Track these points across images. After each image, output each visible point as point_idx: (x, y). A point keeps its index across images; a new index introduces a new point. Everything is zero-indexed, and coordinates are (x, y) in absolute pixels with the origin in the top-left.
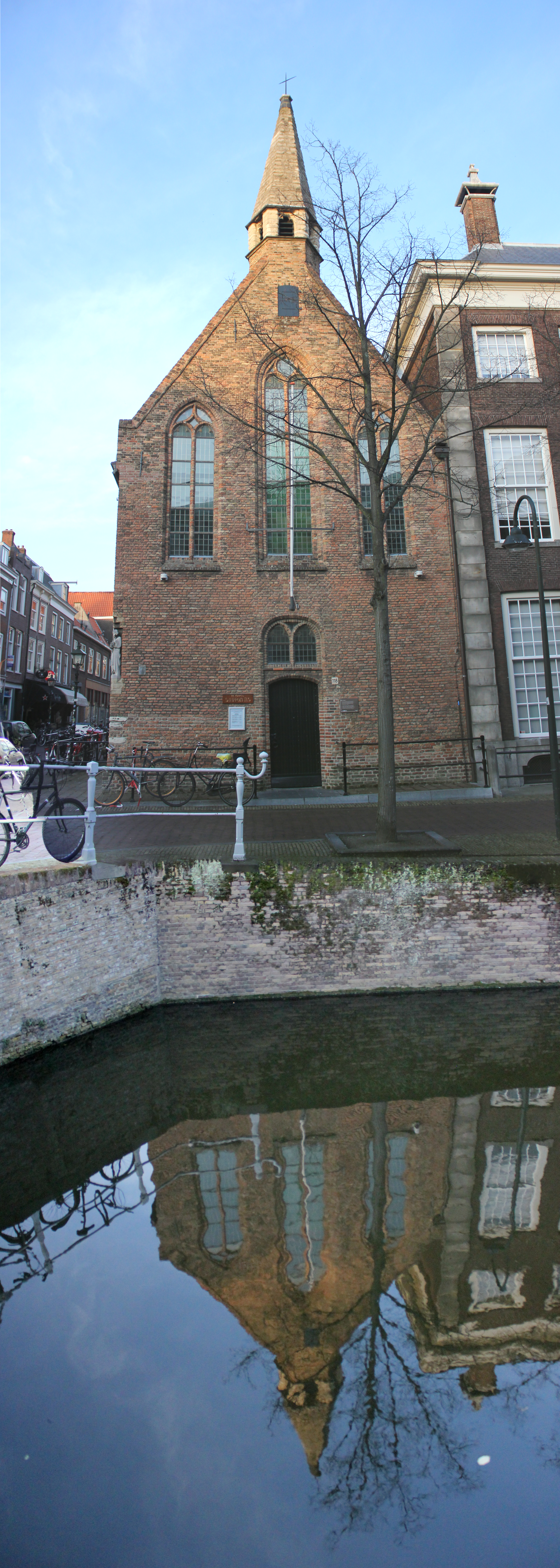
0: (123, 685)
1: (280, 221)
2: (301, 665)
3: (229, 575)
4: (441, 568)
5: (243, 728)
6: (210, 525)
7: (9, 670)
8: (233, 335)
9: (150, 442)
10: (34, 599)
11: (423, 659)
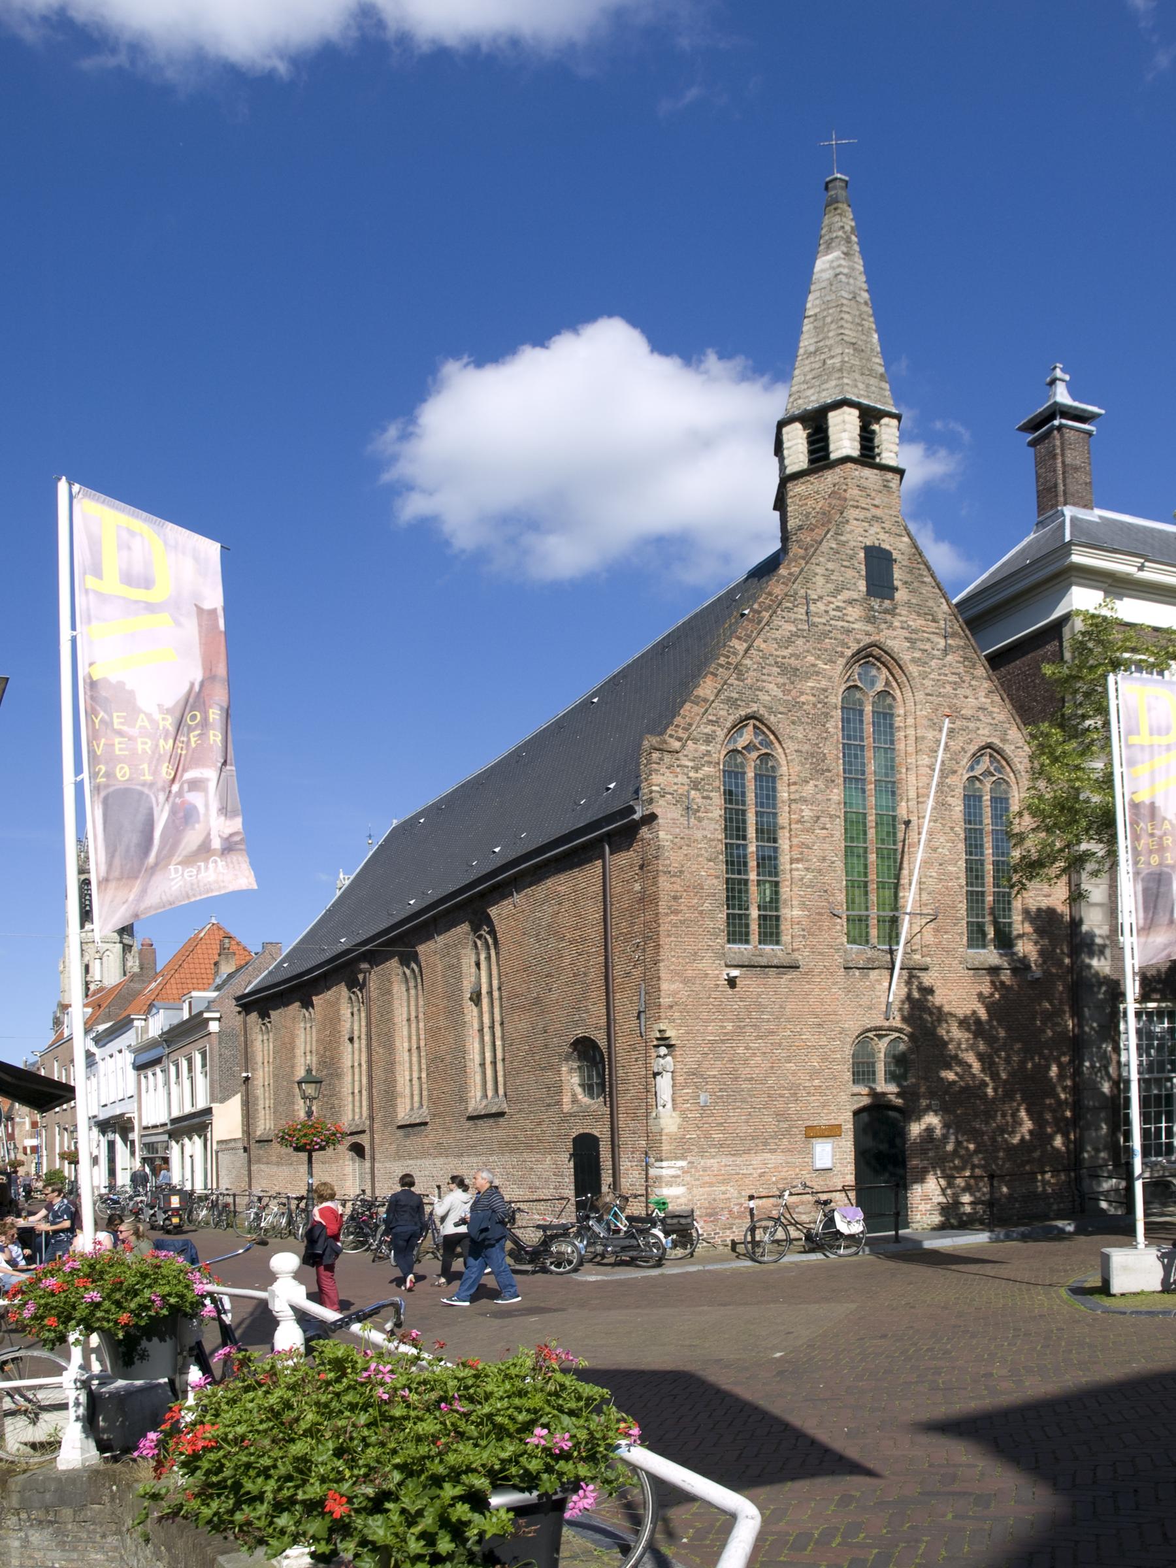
0: (679, 1120)
3: (811, 971)
5: (829, 1165)
8: (804, 617)
9: (699, 775)
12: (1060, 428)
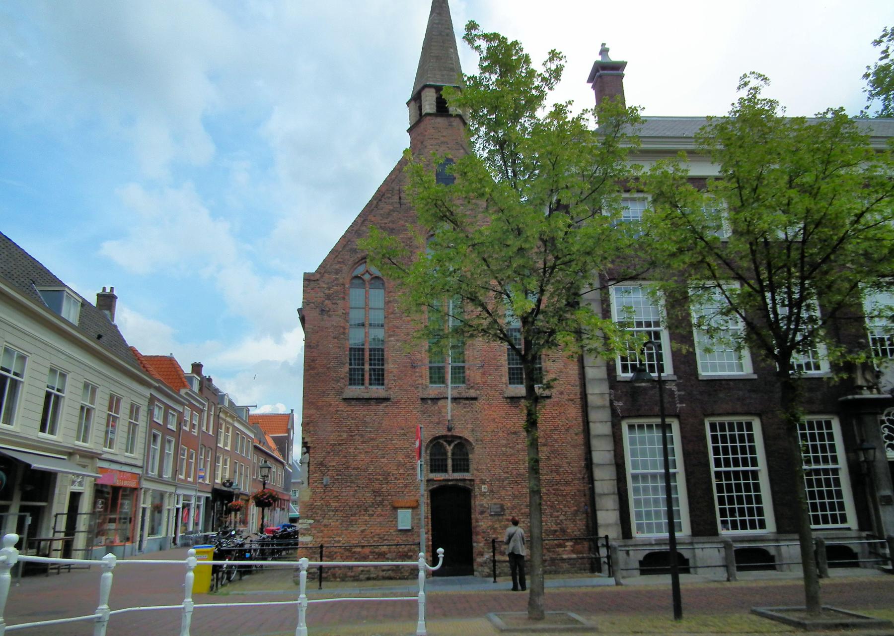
1: (437, 98)
2: (458, 476)
3: (396, 403)
4: (572, 396)
5: (409, 528)
6: (382, 360)
7: (200, 481)
10: (221, 421)
11: (557, 472)
12: (600, 76)
